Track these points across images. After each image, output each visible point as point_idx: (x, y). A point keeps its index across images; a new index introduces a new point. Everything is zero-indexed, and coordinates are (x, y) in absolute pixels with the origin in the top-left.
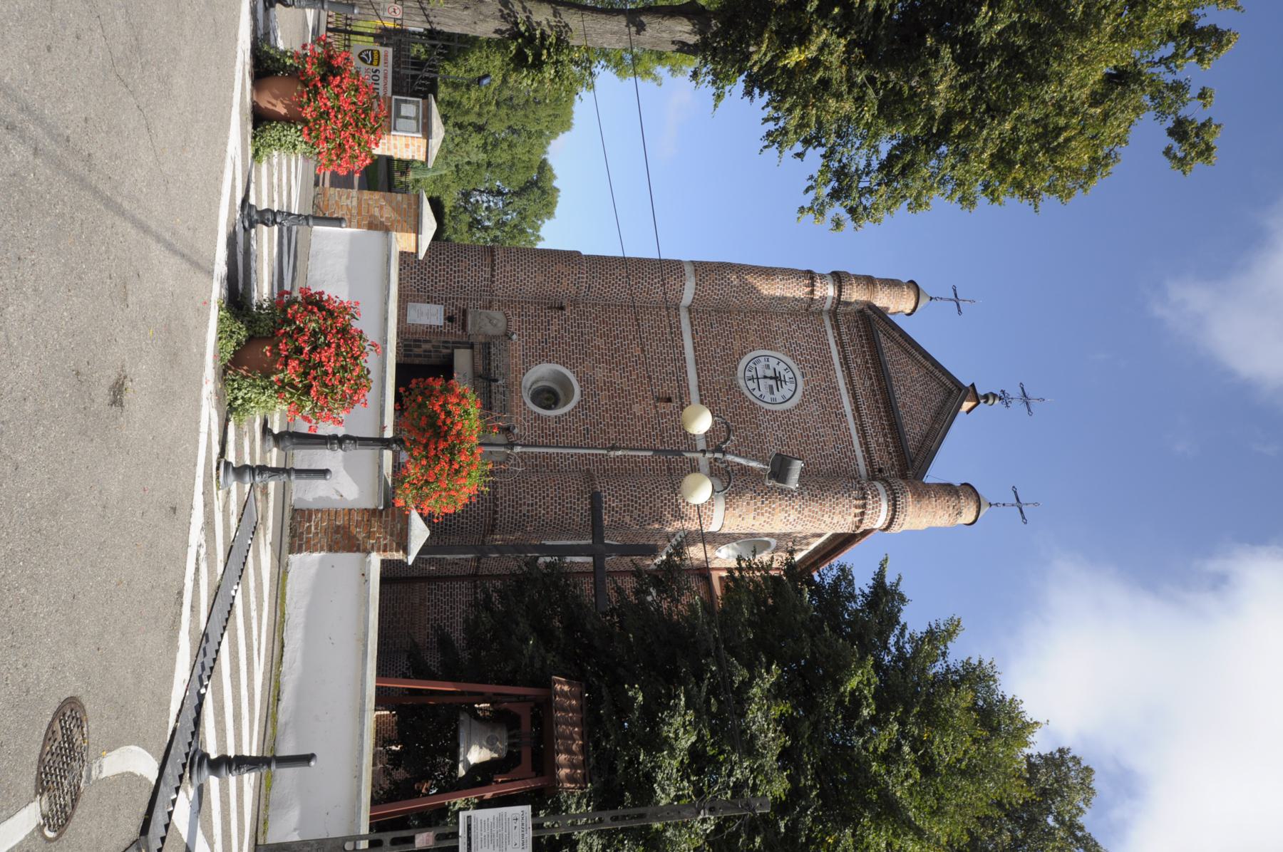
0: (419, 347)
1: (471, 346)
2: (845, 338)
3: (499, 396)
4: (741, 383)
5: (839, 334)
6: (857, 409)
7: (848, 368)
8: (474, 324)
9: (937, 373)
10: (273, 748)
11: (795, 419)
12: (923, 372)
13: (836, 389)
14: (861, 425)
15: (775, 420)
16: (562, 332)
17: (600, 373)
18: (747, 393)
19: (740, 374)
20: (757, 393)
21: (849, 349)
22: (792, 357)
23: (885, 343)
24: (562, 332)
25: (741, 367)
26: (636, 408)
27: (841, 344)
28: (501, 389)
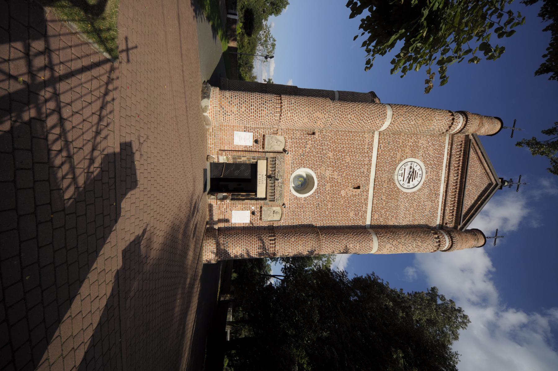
0: (241, 159)
3: (279, 189)
5: (451, 149)
7: (449, 169)
8: (268, 145)
13: (440, 180)
14: (445, 200)
15: (407, 197)
16: (313, 149)
17: (328, 173)
20: (402, 183)
21: (453, 158)
24: (313, 149)
26: (343, 193)
28: (280, 185)
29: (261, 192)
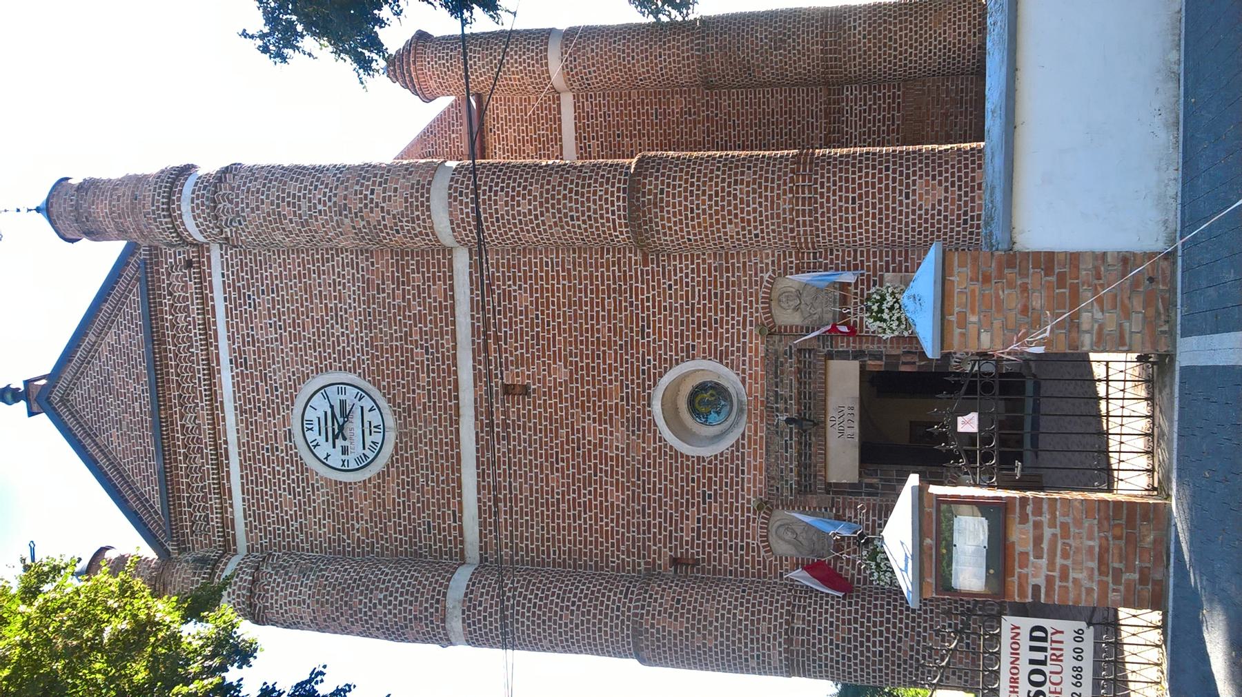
1: (829, 487)
2: (214, 502)
4: (390, 421)
6: (212, 373)
9: (79, 434)
10: (1157, 627)
11: (312, 355)
12: (101, 439)
18: (383, 403)
19: (391, 437)
20: (367, 403)
22: (304, 469)
23: (153, 492)
25: (388, 449)
27: (223, 491)
29: (843, 382)
